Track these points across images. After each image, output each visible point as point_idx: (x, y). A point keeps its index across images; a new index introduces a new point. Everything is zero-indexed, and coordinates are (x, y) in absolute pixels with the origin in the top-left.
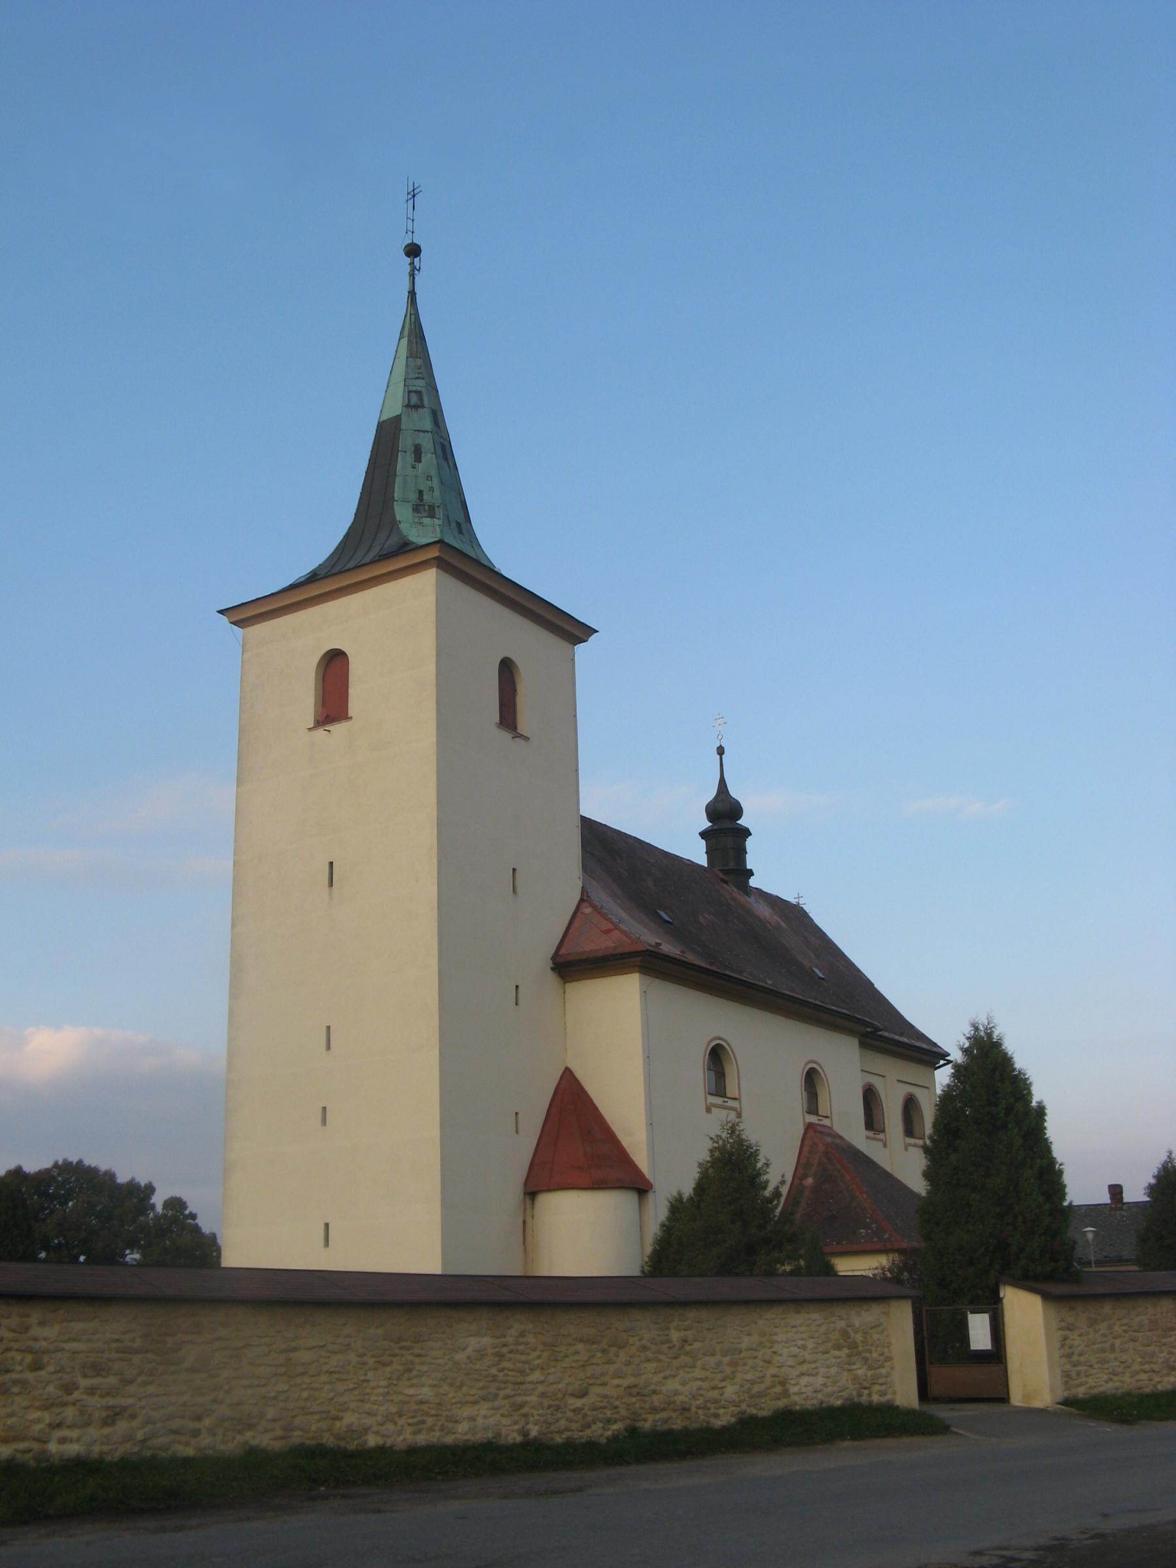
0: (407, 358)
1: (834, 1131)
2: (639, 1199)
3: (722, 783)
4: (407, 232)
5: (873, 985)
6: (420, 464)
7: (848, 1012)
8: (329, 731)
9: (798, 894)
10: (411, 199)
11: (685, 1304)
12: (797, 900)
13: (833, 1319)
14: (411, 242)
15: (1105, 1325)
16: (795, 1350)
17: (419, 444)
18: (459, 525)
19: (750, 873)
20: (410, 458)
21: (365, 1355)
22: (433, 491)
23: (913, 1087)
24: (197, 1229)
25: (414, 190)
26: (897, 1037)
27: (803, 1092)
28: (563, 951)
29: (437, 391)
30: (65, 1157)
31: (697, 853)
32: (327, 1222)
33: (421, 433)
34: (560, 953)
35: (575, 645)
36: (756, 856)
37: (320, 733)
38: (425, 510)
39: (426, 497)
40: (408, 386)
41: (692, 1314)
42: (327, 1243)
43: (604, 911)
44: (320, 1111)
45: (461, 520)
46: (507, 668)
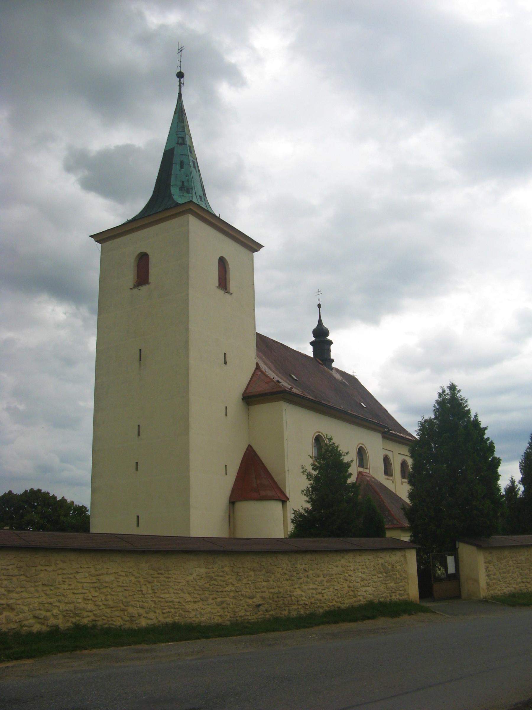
0: (178, 122)
1: (371, 475)
2: (283, 504)
4: (178, 67)
5: (387, 411)
6: (183, 170)
7: (377, 422)
8: (140, 289)
9: (354, 371)
10: (180, 52)
11: (305, 552)
12: (353, 374)
13: (378, 559)
14: (180, 71)
15: (505, 561)
16: (360, 574)
17: (182, 161)
18: (200, 197)
19: (332, 361)
20: (178, 167)
21: (140, 577)
22: (189, 181)
23: (404, 456)
25: (181, 48)
26: (398, 434)
27: (357, 457)
28: (247, 391)
29: (191, 138)
31: (309, 351)
33: (183, 156)
34: (246, 392)
35: (254, 252)
36: (335, 352)
37: (136, 291)
38: (185, 190)
39: (185, 184)
40: (178, 135)
41: (308, 557)
42: (138, 526)
43: (267, 373)
44: (135, 464)
45: (202, 195)
46: (223, 263)
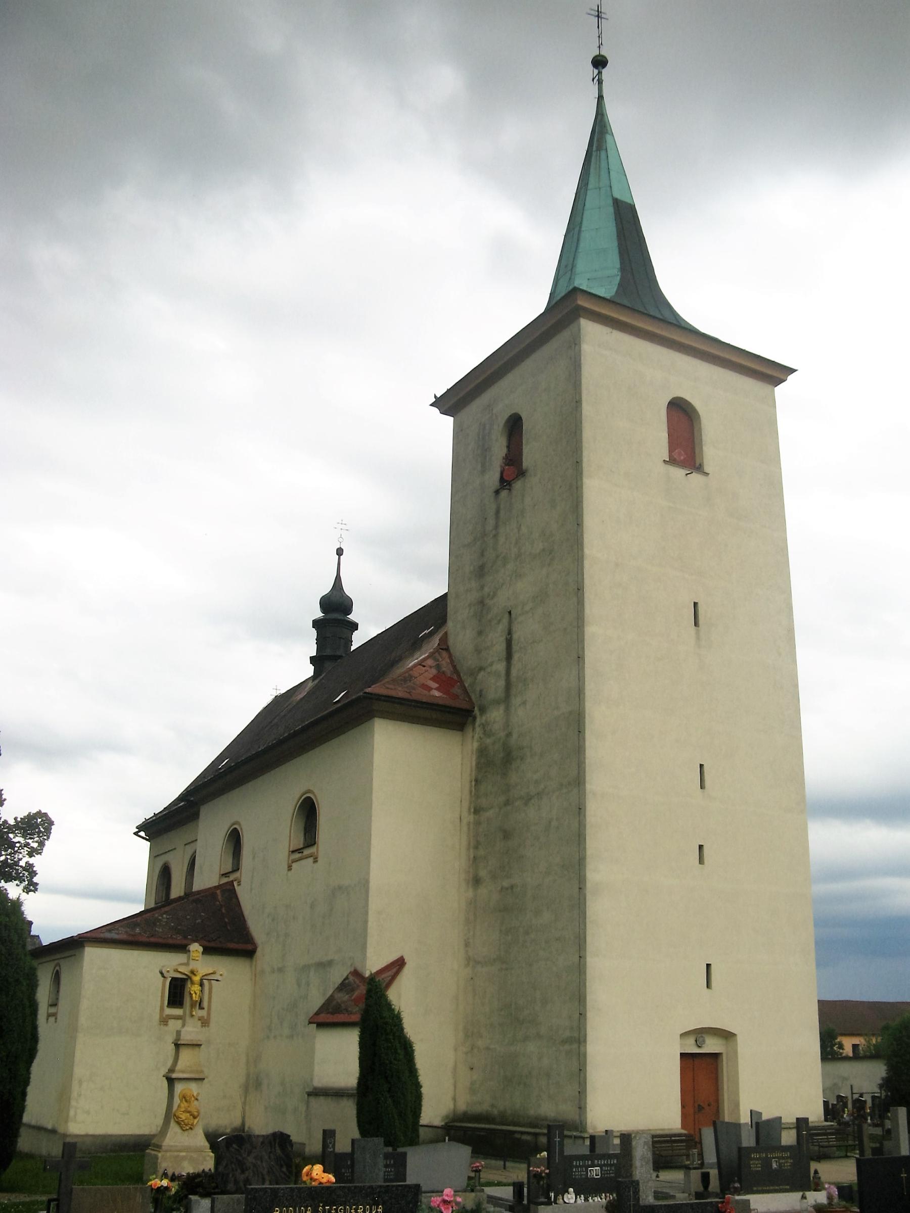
3: (338, 579)
24: (417, 1079)
30: (416, 1050)
32: (709, 990)
